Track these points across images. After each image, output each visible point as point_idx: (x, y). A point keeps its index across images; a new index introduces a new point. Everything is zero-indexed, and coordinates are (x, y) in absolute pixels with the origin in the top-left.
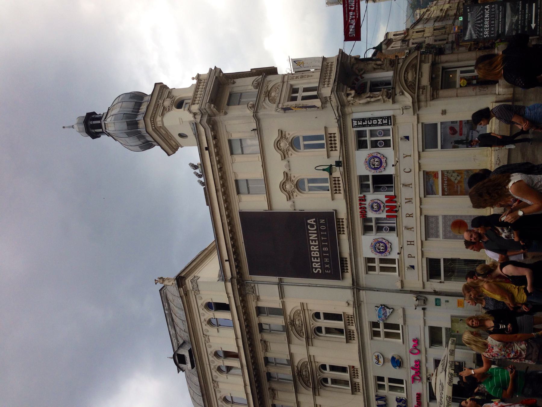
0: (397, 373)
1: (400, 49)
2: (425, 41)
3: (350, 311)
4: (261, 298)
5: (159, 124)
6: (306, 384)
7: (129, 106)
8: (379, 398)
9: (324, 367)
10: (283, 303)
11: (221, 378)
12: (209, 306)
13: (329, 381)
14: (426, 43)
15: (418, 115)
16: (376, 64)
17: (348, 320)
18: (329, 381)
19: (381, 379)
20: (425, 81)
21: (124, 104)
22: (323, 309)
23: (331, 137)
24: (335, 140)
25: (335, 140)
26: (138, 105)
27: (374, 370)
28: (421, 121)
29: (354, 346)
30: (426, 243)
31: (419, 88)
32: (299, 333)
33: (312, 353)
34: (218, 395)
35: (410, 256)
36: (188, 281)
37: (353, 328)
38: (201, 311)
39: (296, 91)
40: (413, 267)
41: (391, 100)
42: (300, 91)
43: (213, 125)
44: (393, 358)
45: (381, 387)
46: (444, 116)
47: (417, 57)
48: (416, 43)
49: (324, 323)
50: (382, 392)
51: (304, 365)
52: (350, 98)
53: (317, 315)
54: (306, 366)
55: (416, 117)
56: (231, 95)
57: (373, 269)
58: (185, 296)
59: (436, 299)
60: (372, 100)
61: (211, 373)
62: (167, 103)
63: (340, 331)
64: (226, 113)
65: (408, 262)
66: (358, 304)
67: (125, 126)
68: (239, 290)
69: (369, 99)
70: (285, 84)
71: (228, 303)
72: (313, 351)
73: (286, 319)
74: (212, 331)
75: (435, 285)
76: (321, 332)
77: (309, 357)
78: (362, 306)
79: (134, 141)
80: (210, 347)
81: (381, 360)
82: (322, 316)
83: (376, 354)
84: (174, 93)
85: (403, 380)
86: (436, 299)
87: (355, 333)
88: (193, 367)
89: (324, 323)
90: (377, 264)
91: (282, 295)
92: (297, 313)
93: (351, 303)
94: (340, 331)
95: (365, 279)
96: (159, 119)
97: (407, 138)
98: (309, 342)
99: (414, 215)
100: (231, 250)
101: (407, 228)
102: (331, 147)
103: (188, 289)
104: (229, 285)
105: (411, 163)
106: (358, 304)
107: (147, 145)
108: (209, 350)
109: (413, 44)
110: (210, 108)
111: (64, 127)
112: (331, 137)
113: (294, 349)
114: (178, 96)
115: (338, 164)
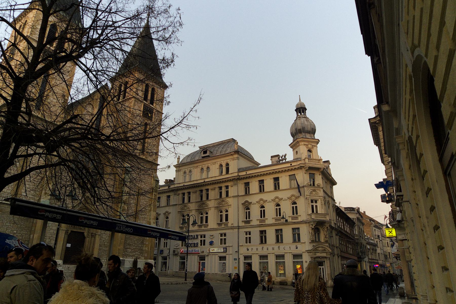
0: (207, 243)
1: (373, 234)
2: (379, 248)
3: (230, 225)
4: (232, 188)
5: (300, 143)
6: (200, 206)
7: (309, 128)
8: (197, 236)
9: (207, 213)
10: (230, 197)
11: (199, 170)
12: (227, 164)
13: (202, 216)
14: (377, 249)
15: (305, 252)
16: (326, 235)
17: (226, 225)
18: (202, 216)
19: (204, 237)
20: (318, 255)
21: (309, 126)
22: (229, 213)
23: (297, 218)
24: (296, 219)
25: (296, 219)
26: (309, 132)
27: (208, 234)
28: (303, 253)
29: (216, 226)
30: (257, 255)
31: (315, 252)
32: (219, 204)
33: (212, 209)
34: (192, 168)
35: (252, 249)
36: (236, 156)
37: (223, 226)
38: (225, 161)
39: (316, 202)
40: (248, 250)
41: (311, 242)
42: (316, 204)
43: (301, 168)
44: (213, 242)
45: (201, 237)
46: (305, 262)
47: (329, 251)
48: (377, 243)
49: (224, 214)
50: (199, 237)
51: (207, 206)
52: (311, 226)
53: (227, 211)
54: (206, 206)
55: (305, 251)
56: (314, 174)
57: (246, 234)
58: (230, 154)
59: (236, 259)
60: (311, 235)
61: (200, 165)
62: (310, 146)
63: (221, 220)
64: (305, 173)
65: (250, 249)
66: (232, 228)
67: (299, 128)
68: (235, 179)
69: (311, 233)
70: (319, 197)
71: (229, 173)
72: (213, 209)
73: (225, 198)
74: (217, 166)
75: (242, 258)
76: (220, 213)
77: (210, 208)
78: (232, 230)
79: (294, 131)
80: (211, 165)
81: (212, 237)
82: (227, 213)
83: (214, 235)
84: (315, 148)
85: (205, 238)
86: (236, 259)
87: (221, 227)
88: (203, 157)
89: (224, 214)
90: (248, 236)
91: (233, 197)
92: (227, 203)
93: (232, 226)
94: (221, 220)
95: (242, 231)
96: (303, 143)
97: (297, 248)
98: (216, 208)
99: (268, 251)
100: (251, 175)
101: (263, 248)
102: (293, 218)
103: (234, 156)
104: (236, 174)
105: (287, 250)
106: (232, 228)
107: (293, 135)
108: (209, 164)
109: (377, 241)
110: (307, 167)
111: (300, 96)
112: (297, 218)
113: (213, 201)
114: (313, 150)
115: (286, 221)
